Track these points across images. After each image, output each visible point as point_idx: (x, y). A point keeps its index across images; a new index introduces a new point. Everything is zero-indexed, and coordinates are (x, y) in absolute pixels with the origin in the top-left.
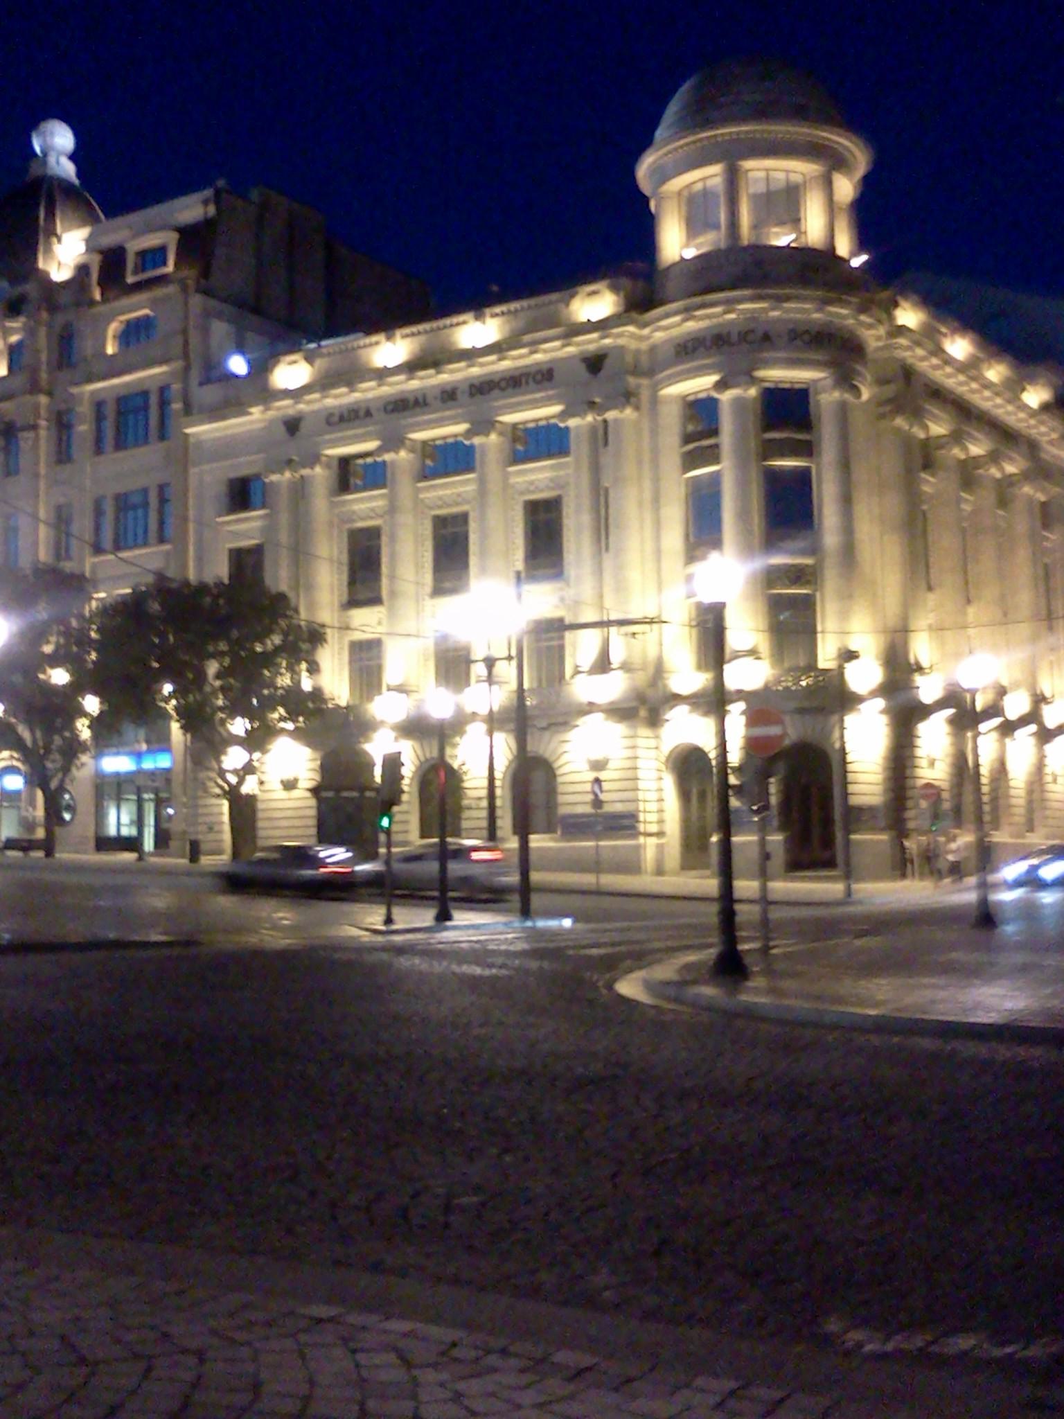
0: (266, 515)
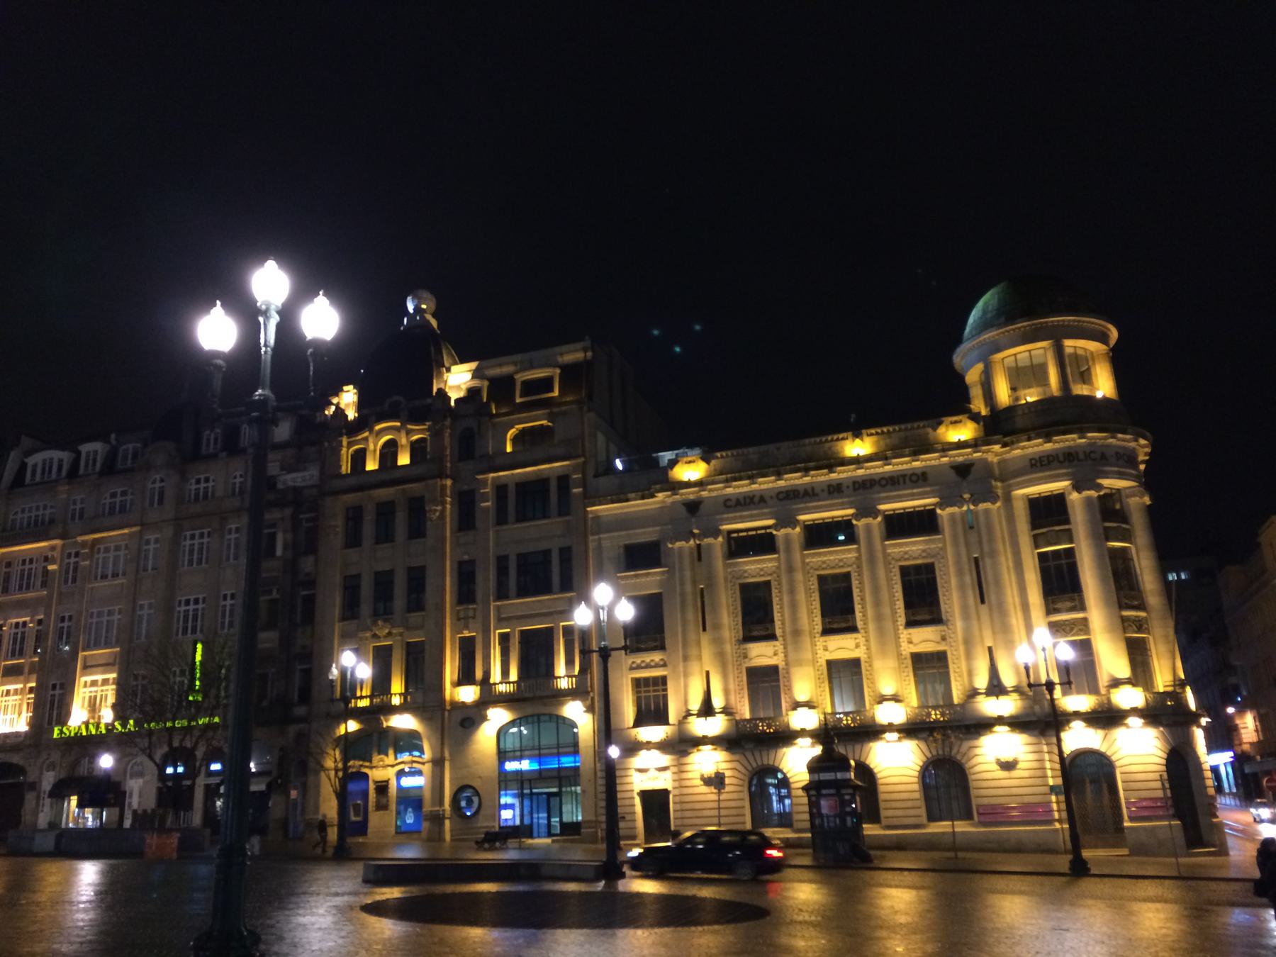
0: (667, 572)
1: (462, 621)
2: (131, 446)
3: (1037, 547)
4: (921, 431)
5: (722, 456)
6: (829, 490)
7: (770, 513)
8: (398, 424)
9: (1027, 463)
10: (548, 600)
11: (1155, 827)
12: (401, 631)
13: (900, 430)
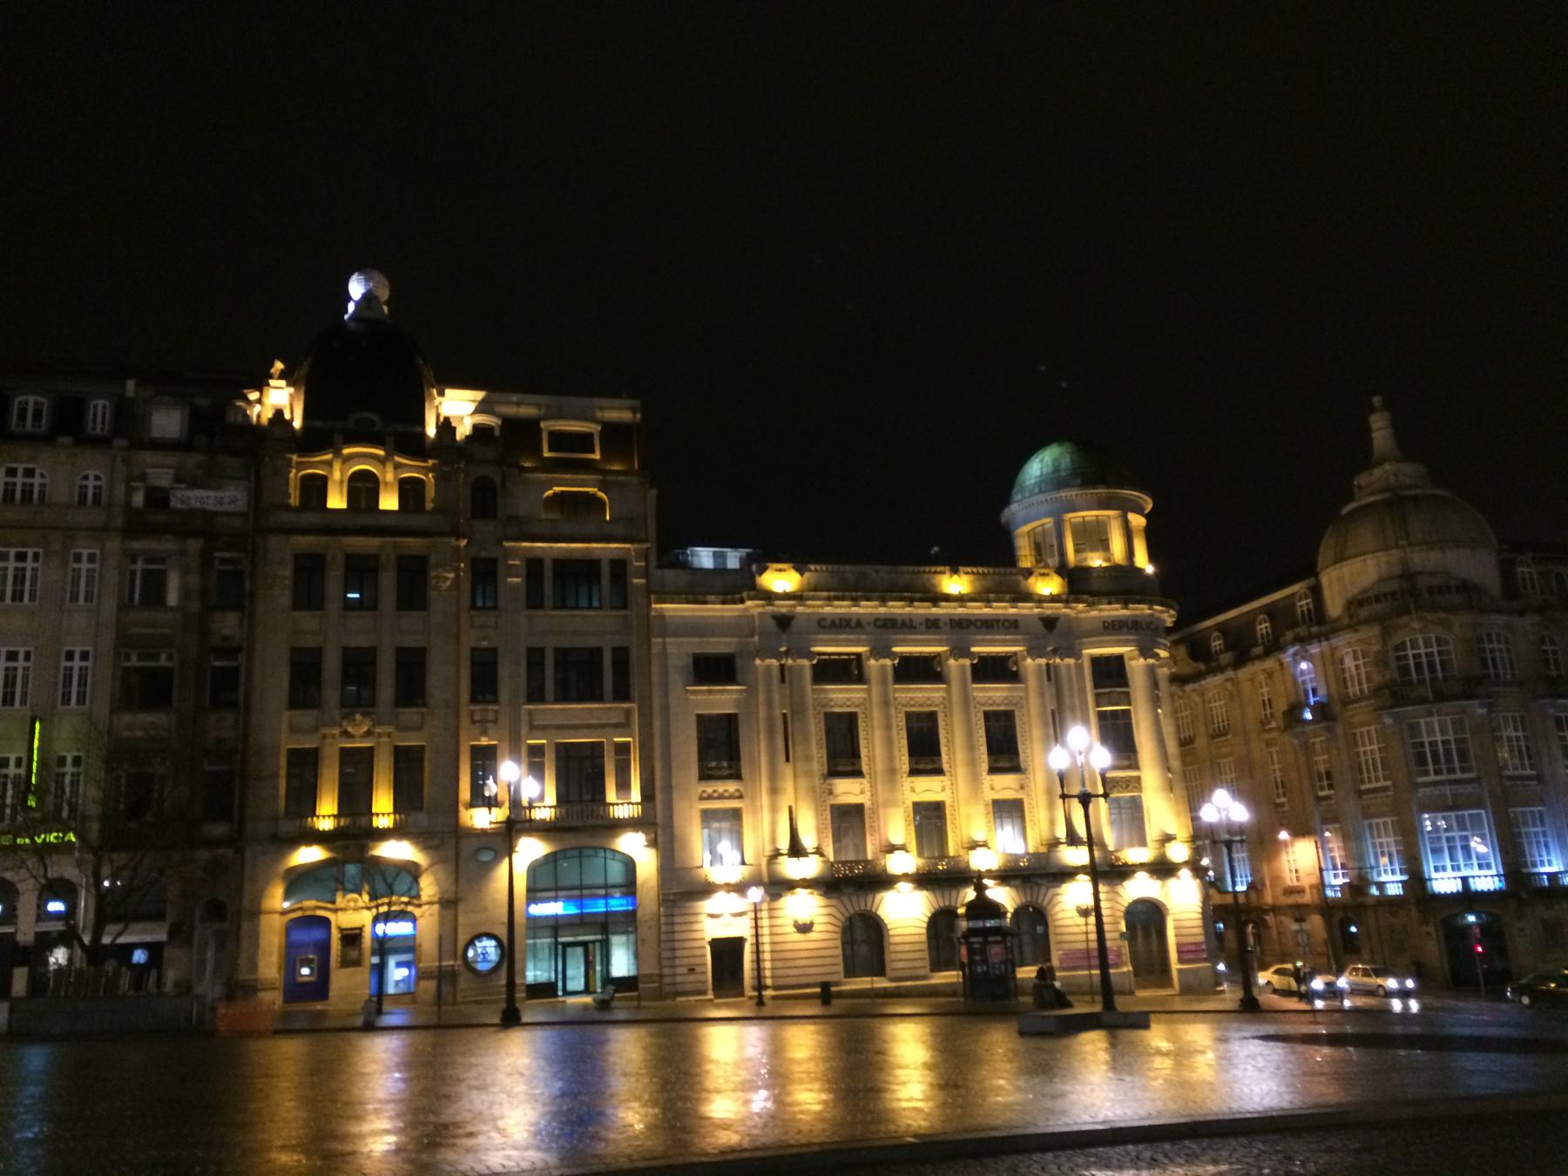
0: (745, 691)
1: (478, 725)
2: (31, 399)
3: (1098, 706)
4: (1013, 577)
5: (822, 570)
6: (951, 624)
7: (1133, 641)
8: (381, 453)
9: (1101, 625)
10: (598, 709)
11: (1198, 968)
12: (390, 730)
13: (994, 573)
